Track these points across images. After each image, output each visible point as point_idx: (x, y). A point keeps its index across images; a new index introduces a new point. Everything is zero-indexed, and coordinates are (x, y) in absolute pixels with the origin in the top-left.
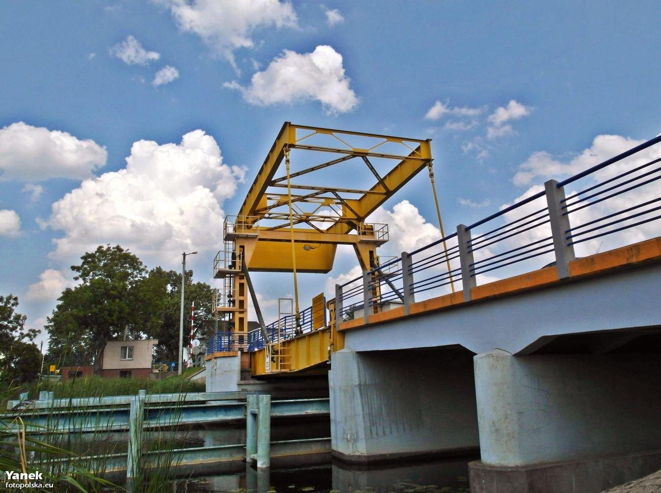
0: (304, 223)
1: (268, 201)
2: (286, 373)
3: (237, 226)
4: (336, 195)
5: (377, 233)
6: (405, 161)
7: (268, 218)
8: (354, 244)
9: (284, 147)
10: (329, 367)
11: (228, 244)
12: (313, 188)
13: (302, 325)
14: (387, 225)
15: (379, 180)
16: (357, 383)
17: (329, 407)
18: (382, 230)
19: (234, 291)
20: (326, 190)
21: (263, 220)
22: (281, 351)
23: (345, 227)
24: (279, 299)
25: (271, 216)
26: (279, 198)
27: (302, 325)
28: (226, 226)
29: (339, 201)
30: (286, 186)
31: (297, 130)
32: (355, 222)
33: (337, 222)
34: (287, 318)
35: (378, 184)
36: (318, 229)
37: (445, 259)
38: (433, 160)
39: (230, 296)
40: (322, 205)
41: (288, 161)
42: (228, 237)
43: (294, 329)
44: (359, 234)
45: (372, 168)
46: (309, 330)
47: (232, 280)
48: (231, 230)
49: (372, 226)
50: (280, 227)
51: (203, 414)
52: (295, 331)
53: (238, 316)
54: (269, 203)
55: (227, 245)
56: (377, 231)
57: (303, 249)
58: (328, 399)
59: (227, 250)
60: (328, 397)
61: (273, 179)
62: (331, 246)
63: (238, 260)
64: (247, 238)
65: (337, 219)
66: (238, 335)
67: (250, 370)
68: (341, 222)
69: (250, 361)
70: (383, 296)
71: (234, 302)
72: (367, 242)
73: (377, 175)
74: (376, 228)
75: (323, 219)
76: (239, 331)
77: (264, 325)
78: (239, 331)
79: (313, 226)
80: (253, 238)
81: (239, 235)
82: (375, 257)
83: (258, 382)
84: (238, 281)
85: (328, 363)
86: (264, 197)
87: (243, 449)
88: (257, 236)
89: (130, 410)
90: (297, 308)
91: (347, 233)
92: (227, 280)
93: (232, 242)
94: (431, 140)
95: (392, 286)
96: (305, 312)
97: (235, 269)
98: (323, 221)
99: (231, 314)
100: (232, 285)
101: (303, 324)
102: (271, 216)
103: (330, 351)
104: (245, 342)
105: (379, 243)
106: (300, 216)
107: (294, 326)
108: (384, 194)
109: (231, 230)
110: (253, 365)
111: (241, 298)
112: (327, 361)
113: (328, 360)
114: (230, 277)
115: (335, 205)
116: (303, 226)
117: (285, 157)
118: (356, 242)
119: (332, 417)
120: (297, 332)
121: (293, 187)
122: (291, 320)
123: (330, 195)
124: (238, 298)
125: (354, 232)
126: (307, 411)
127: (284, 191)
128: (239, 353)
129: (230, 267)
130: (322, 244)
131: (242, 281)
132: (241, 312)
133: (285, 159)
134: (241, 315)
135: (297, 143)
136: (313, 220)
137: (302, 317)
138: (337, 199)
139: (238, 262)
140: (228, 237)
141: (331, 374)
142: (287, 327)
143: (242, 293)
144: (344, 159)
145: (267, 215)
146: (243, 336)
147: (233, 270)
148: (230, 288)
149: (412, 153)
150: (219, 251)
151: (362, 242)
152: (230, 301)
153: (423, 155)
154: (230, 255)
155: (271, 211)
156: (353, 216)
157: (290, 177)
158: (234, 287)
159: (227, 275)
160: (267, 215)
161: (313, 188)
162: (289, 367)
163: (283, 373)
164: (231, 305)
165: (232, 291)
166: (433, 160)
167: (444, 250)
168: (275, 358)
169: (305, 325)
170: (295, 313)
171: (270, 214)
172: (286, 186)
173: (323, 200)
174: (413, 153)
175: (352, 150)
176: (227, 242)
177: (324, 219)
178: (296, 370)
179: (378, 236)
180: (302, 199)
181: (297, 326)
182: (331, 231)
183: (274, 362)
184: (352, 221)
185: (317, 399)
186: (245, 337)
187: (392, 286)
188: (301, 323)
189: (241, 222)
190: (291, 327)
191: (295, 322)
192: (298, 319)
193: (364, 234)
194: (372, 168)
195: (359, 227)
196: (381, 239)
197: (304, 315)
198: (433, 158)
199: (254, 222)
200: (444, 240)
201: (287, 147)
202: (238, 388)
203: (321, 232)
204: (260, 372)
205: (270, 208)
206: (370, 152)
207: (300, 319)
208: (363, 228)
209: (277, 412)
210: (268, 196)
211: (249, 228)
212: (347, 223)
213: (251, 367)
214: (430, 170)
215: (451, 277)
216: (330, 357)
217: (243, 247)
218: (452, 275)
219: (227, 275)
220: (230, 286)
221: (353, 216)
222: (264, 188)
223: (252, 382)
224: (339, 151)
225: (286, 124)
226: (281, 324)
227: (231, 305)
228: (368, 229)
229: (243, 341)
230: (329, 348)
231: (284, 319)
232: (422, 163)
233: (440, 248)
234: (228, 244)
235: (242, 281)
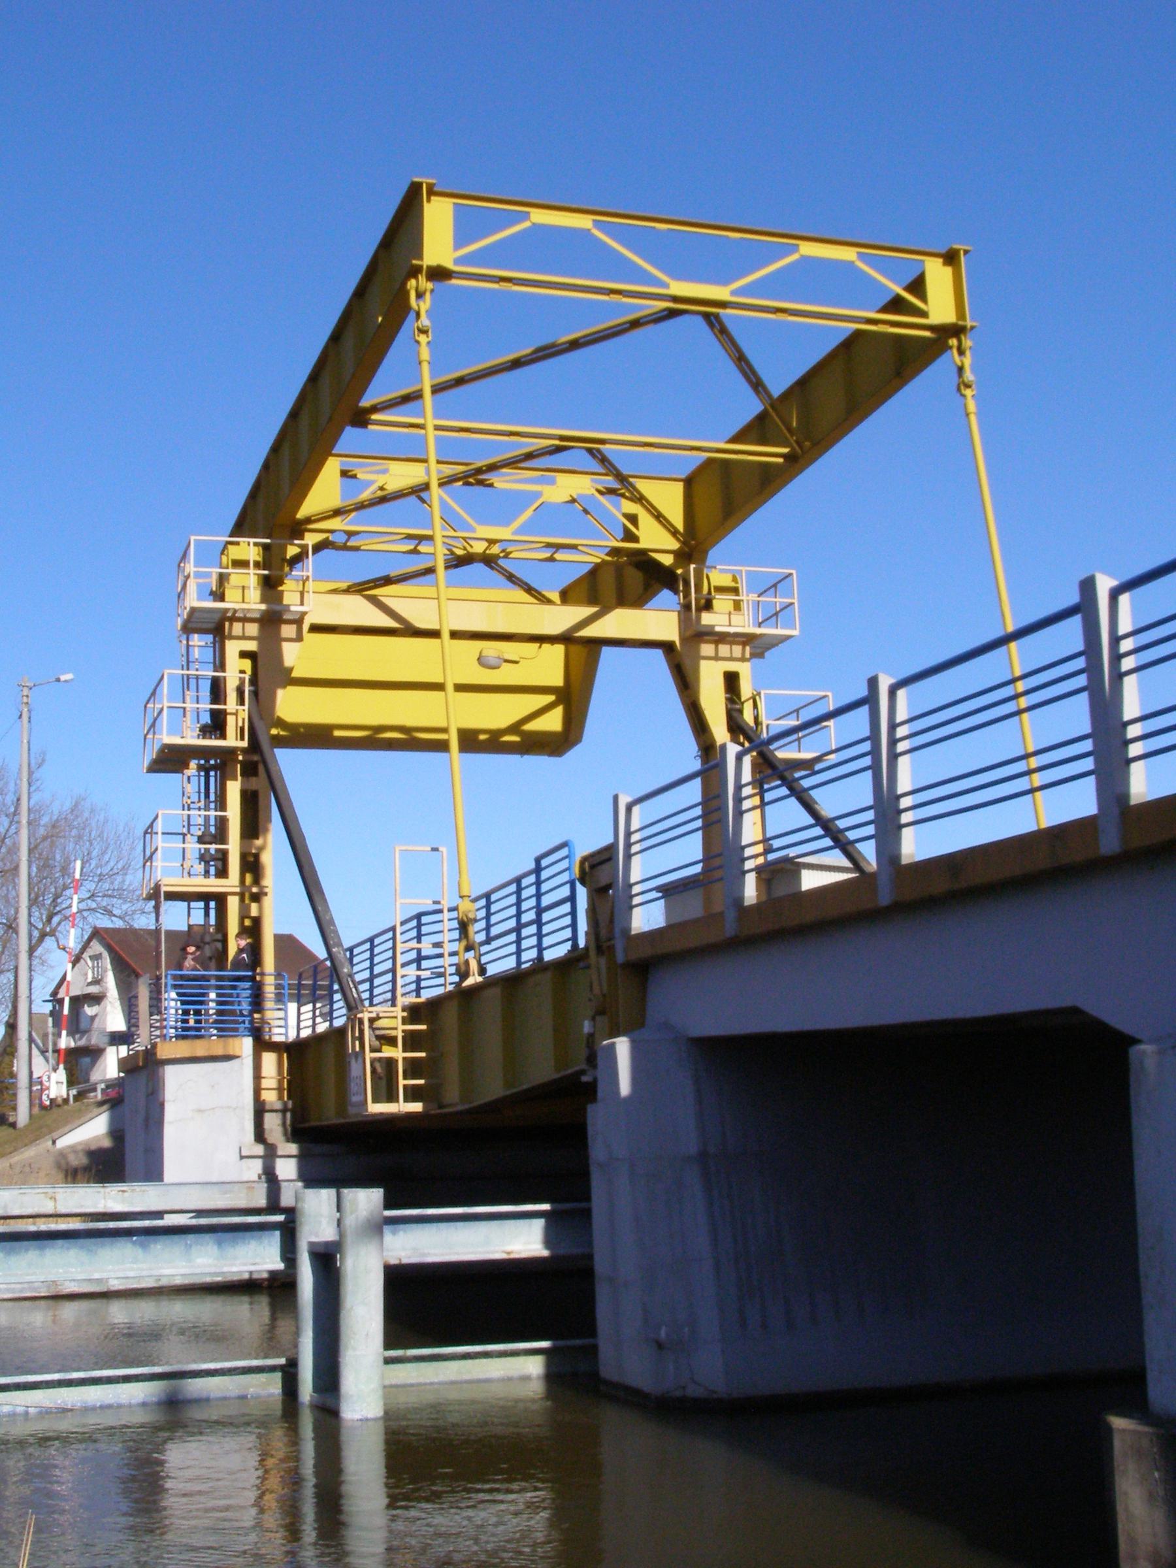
16: (693, 1150)
34: (424, 919)
46: (510, 964)
47: (212, 780)
57: (476, 663)
58: (583, 1205)
60: (588, 1198)
70: (776, 844)
73: (757, 385)
77: (340, 944)
81: (235, 611)
85: (585, 1079)
89: (614, 945)
95: (809, 806)
99: (212, 904)
103: (591, 1036)
112: (583, 1072)
113: (584, 1066)
119: (601, 1266)
126: (509, 1248)
130: (546, 646)
169: (495, 944)
178: (460, 1108)
187: (809, 806)
197: (538, 883)
198: (969, 323)
230: (587, 1027)
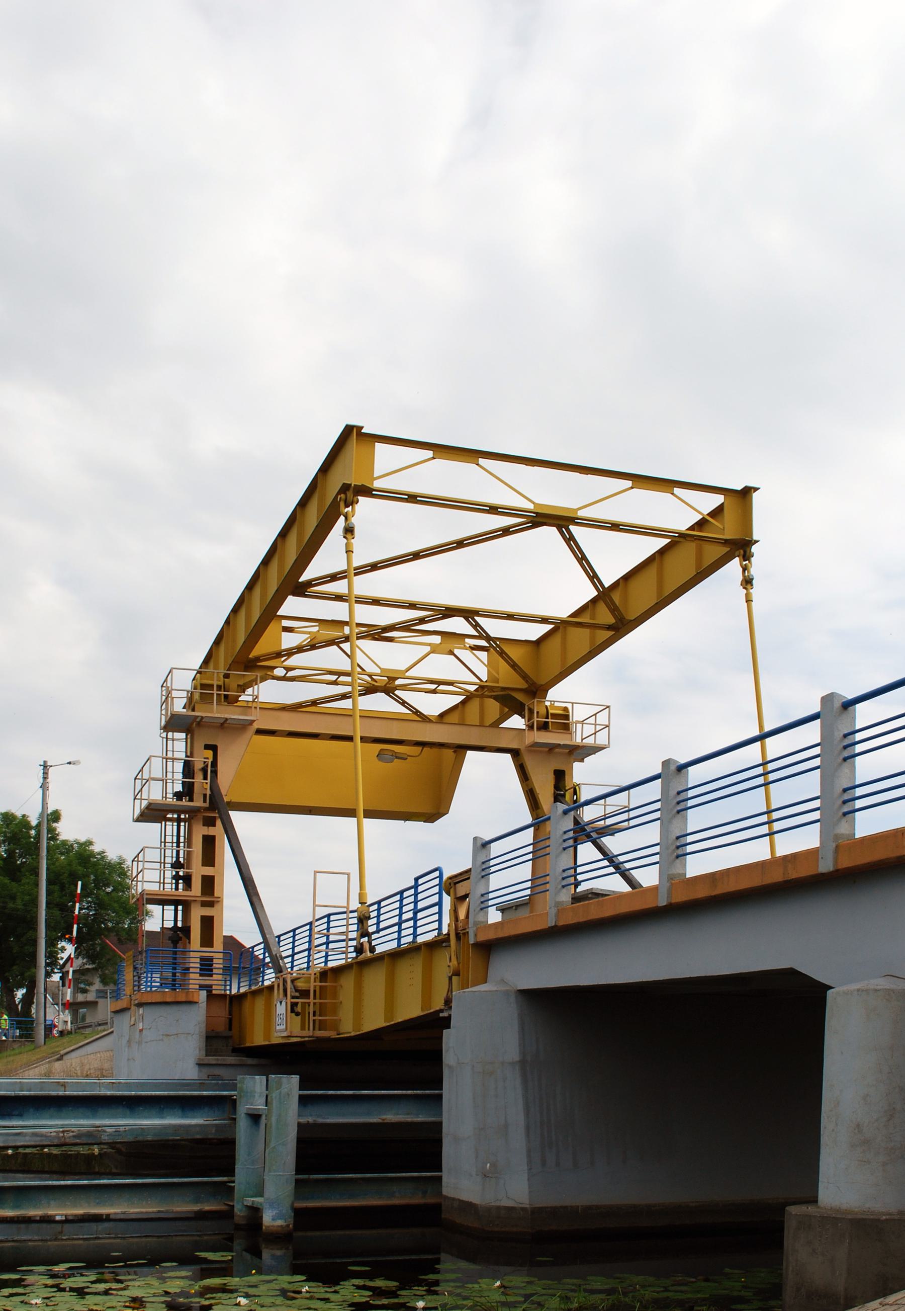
0: (381, 696)
1: (284, 634)
2: (328, 1040)
3: (197, 696)
4: (476, 626)
5: (579, 726)
6: (678, 540)
7: (284, 678)
8: (515, 754)
9: (339, 493)
10: (446, 1023)
11: (173, 740)
12: (412, 606)
13: (374, 933)
14: (608, 707)
15: (598, 592)
17: (442, 1109)
18: (592, 720)
19: (189, 855)
20: (449, 612)
21: (270, 682)
22: (315, 991)
23: (493, 707)
24: (316, 872)
25: (290, 674)
26: (316, 629)
27: (374, 933)
28: (169, 693)
29: (483, 643)
30: (339, 598)
31: (379, 446)
32: (520, 697)
33: (469, 697)
34: (332, 918)
35: (594, 601)
36: (417, 712)
37: (765, 829)
38: (756, 542)
39: (177, 865)
40: (433, 651)
41: (349, 531)
42: (173, 724)
43: (354, 943)
44: (530, 727)
45: (582, 559)
46: (393, 945)
47: (182, 828)
48: (179, 706)
49: (566, 709)
50: (314, 703)
51: (128, 1112)
52: (355, 947)
53: (197, 913)
54: (288, 641)
55: (170, 742)
56: (577, 722)
59: (170, 755)
61: (304, 578)
62: (449, 753)
63: (198, 779)
64: (224, 725)
65: (472, 688)
66: (198, 955)
67: (229, 1034)
68: (482, 696)
69: (230, 1013)
71: (187, 880)
72: (551, 748)
74: (578, 714)
75: (433, 687)
76: (202, 946)
78: (202, 946)
79: (403, 703)
80: (244, 726)
81: (202, 718)
82: (568, 785)
83: (250, 1061)
84: (200, 831)
86: (272, 627)
87: (227, 1190)
88: (254, 721)
90: (362, 897)
91: (496, 724)
92: (169, 828)
93: (183, 735)
94: (756, 489)
96: (383, 904)
97: (191, 800)
98: (434, 692)
99: (180, 908)
100: (182, 839)
101: (378, 931)
102: (290, 674)
104: (215, 971)
105: (581, 752)
106: (370, 676)
107: (353, 935)
108: (609, 628)
109: (179, 706)
110: (235, 1024)
111: (208, 871)
112: (441, 1011)
113: (443, 1007)
114: (179, 820)
115: (468, 652)
116: (379, 703)
117: (342, 518)
118: (522, 748)
120: (359, 950)
121: (362, 600)
122: (344, 923)
123: (458, 625)
124: (198, 871)
125: (516, 722)
126: (384, 1117)
127: (338, 610)
128: (203, 994)
129: (178, 795)
131: (211, 831)
132: (205, 904)
133: (341, 523)
134: (207, 912)
135: (377, 484)
136: (404, 687)
137: (374, 914)
138: (479, 637)
139: (200, 783)
140: (173, 724)
141: (449, 1038)
142: (332, 938)
143: (209, 857)
144: (506, 531)
145: (279, 672)
146: (211, 959)
147: (185, 802)
148: (178, 846)
149: (696, 523)
150: (151, 756)
151: (535, 747)
152: (176, 878)
153: (728, 529)
154: (179, 767)
155: (293, 661)
156: (517, 682)
157: (356, 574)
158: (189, 842)
159: (169, 816)
160: (279, 672)
161: (412, 606)
162: (335, 1026)
163: (319, 1040)
164: (181, 886)
165: (181, 854)
166: (756, 542)
167: (765, 810)
168: (299, 1006)
169: (382, 933)
170: (355, 905)
171: (288, 669)
172: (339, 598)
173: (437, 639)
174: (701, 524)
175: (530, 506)
176: (170, 735)
177: (437, 685)
178: (353, 1034)
179: (581, 735)
180: (379, 634)
181: (362, 936)
182: (454, 717)
183: (297, 1014)
184: (516, 695)
185: (409, 1092)
186: (215, 961)
188: (372, 929)
189: (210, 687)
190: (344, 937)
191: (355, 927)
192: (363, 920)
193: (544, 727)
194: (582, 559)
195: (531, 711)
196: (590, 741)
199: (243, 689)
200: (762, 737)
201: (350, 494)
202: (200, 1071)
203: (424, 719)
204: (258, 1039)
205: (290, 653)
206: (581, 514)
207: (369, 918)
208: (543, 711)
209: (311, 1116)
210: (285, 623)
211: (230, 700)
212: (496, 698)
213: (230, 1029)
214: (744, 570)
215: (770, 822)
216: (448, 1002)
217: (214, 748)
218: (775, 829)
219: (169, 816)
220: (178, 842)
221: (517, 682)
222: (278, 600)
223: (231, 1060)
224: (493, 510)
225: (349, 431)
226: (317, 929)
227: (181, 886)
228: (555, 716)
229: (212, 970)
231: (325, 920)
232: (725, 550)
233: (752, 754)
234: (173, 740)
235: (211, 831)
